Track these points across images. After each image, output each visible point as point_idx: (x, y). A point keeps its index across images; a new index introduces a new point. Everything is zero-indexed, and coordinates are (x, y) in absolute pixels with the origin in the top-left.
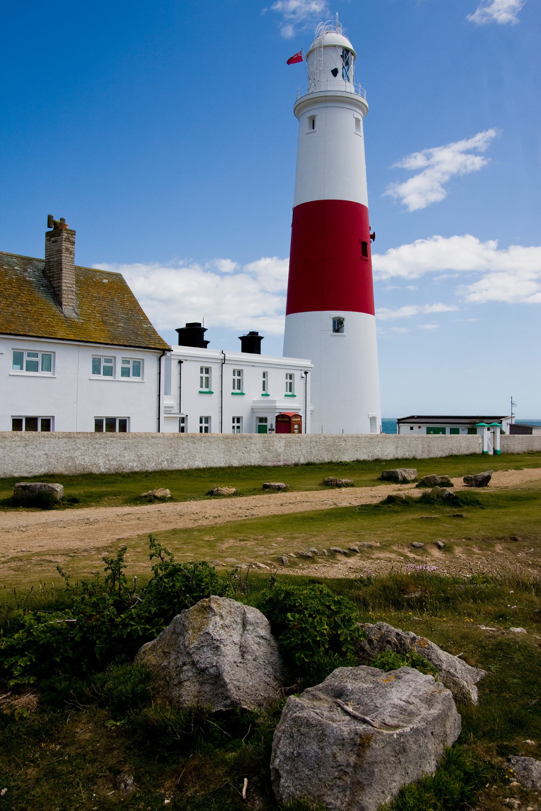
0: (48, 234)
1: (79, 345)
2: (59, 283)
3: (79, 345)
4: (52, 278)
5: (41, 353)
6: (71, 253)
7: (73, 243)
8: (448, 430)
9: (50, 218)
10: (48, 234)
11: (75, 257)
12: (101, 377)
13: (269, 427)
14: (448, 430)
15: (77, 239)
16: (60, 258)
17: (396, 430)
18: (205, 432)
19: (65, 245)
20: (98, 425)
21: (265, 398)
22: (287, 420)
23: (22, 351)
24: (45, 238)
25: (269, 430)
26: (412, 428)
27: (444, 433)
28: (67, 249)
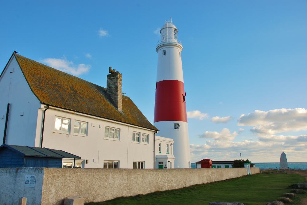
0: (108, 76)
1: (129, 126)
2: (115, 97)
3: (129, 126)
4: (111, 95)
5: (110, 128)
6: (120, 84)
7: (121, 80)
8: (217, 167)
9: (110, 68)
10: (108, 76)
11: (122, 86)
12: (135, 142)
13: (164, 166)
14: (217, 167)
15: (123, 78)
16: (116, 86)
17: (195, 167)
18: (141, 168)
19: (119, 80)
20: (105, 166)
21: (160, 154)
22: (208, 162)
23: (113, 128)
24: (107, 77)
25: (164, 167)
26: (164, 52)
27: (215, 167)
28: (119, 82)
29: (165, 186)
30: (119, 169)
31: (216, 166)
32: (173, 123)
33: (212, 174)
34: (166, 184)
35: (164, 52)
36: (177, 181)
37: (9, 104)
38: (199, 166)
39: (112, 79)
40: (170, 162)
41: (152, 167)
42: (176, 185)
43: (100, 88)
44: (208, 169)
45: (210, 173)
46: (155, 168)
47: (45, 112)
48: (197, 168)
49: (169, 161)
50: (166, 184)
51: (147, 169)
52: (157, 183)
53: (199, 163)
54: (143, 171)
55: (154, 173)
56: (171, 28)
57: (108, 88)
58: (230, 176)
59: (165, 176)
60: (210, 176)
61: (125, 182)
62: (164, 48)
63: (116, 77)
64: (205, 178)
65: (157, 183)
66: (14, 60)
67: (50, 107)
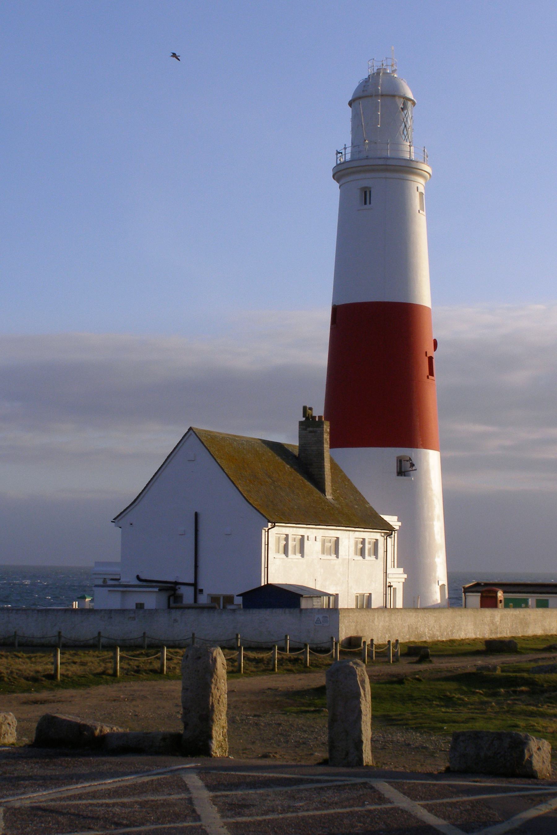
10: (301, 423)
26: (366, 195)
29: (425, 634)
30: (301, 610)
31: (532, 599)
32: (389, 455)
33: (501, 619)
34: (427, 630)
35: (366, 195)
36: (440, 627)
37: (196, 514)
38: (475, 599)
39: (311, 432)
40: (392, 588)
41: (401, 607)
42: (438, 633)
43: (278, 448)
44: (494, 609)
45: (497, 619)
46: (392, 607)
47: (268, 532)
48: (468, 604)
49: (390, 586)
50: (427, 630)
51: (375, 609)
52: (416, 628)
53: (473, 589)
54: (369, 610)
55: (449, 613)
56: (394, 96)
57: (302, 447)
58: (547, 628)
59: (425, 619)
60: (498, 623)
61: (387, 624)
62: (365, 180)
63: (320, 429)
64: (487, 627)
65: (416, 628)
66: (193, 438)
67: (276, 524)
